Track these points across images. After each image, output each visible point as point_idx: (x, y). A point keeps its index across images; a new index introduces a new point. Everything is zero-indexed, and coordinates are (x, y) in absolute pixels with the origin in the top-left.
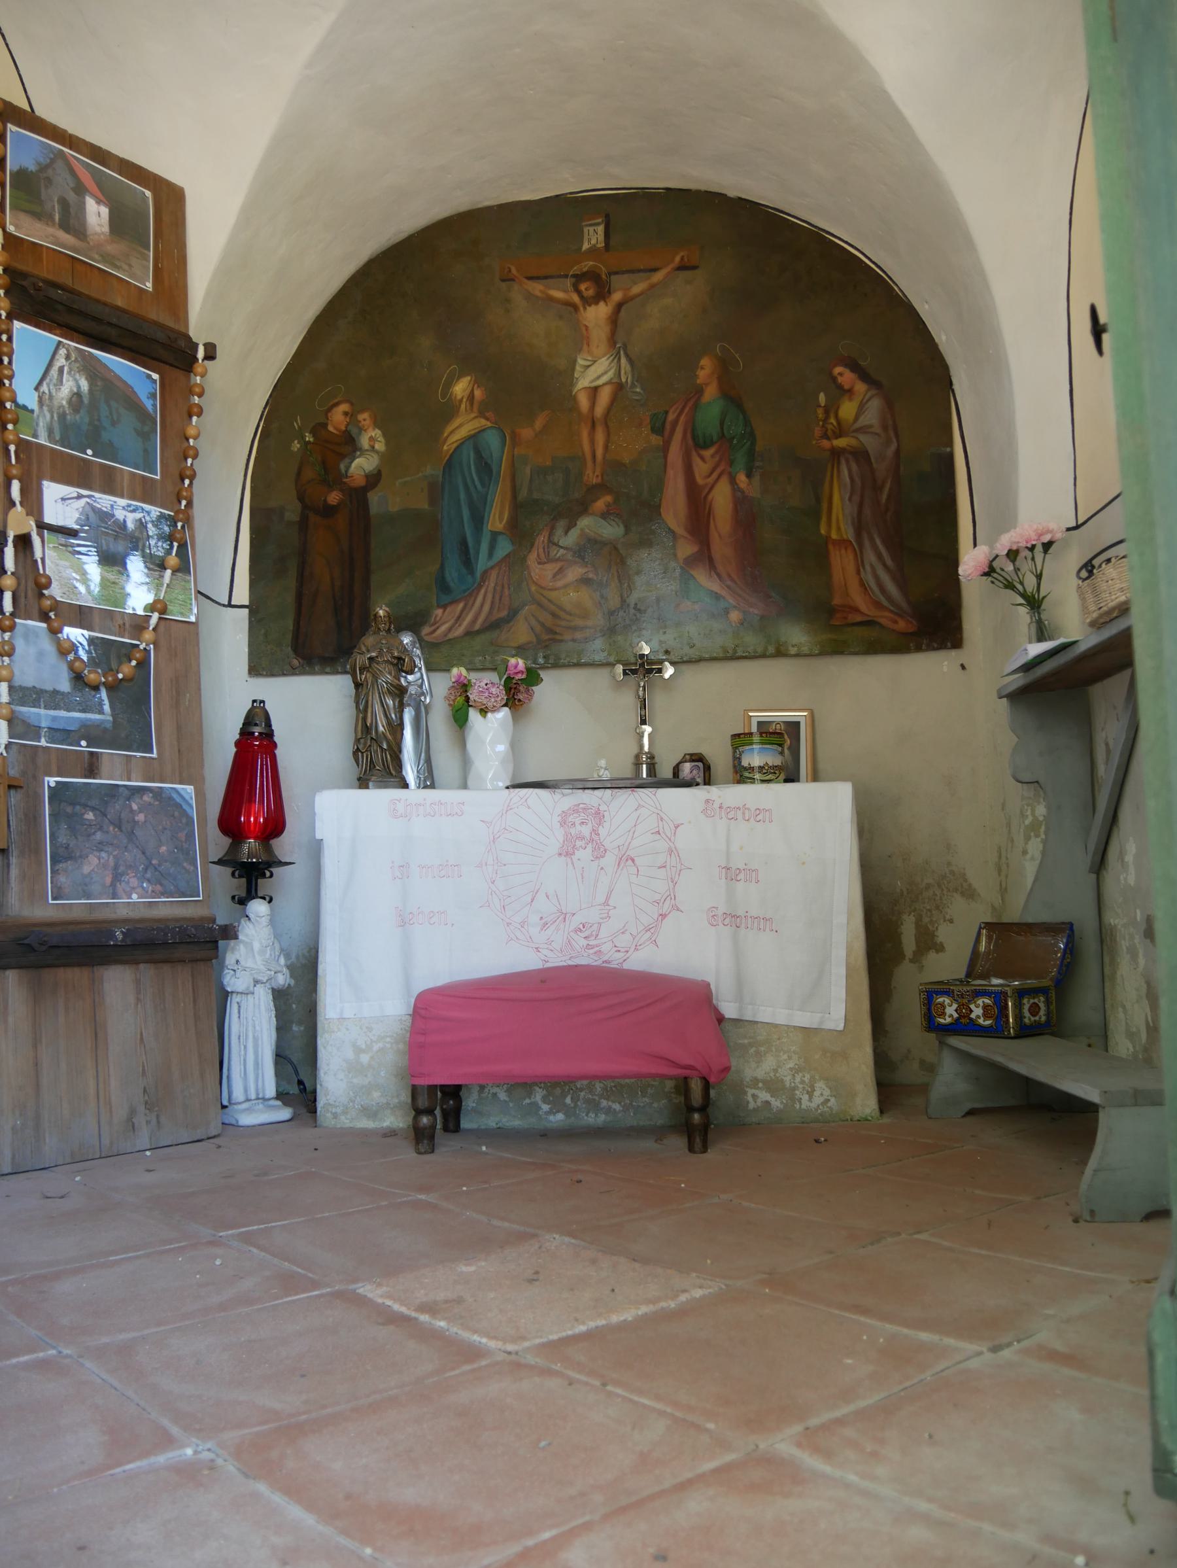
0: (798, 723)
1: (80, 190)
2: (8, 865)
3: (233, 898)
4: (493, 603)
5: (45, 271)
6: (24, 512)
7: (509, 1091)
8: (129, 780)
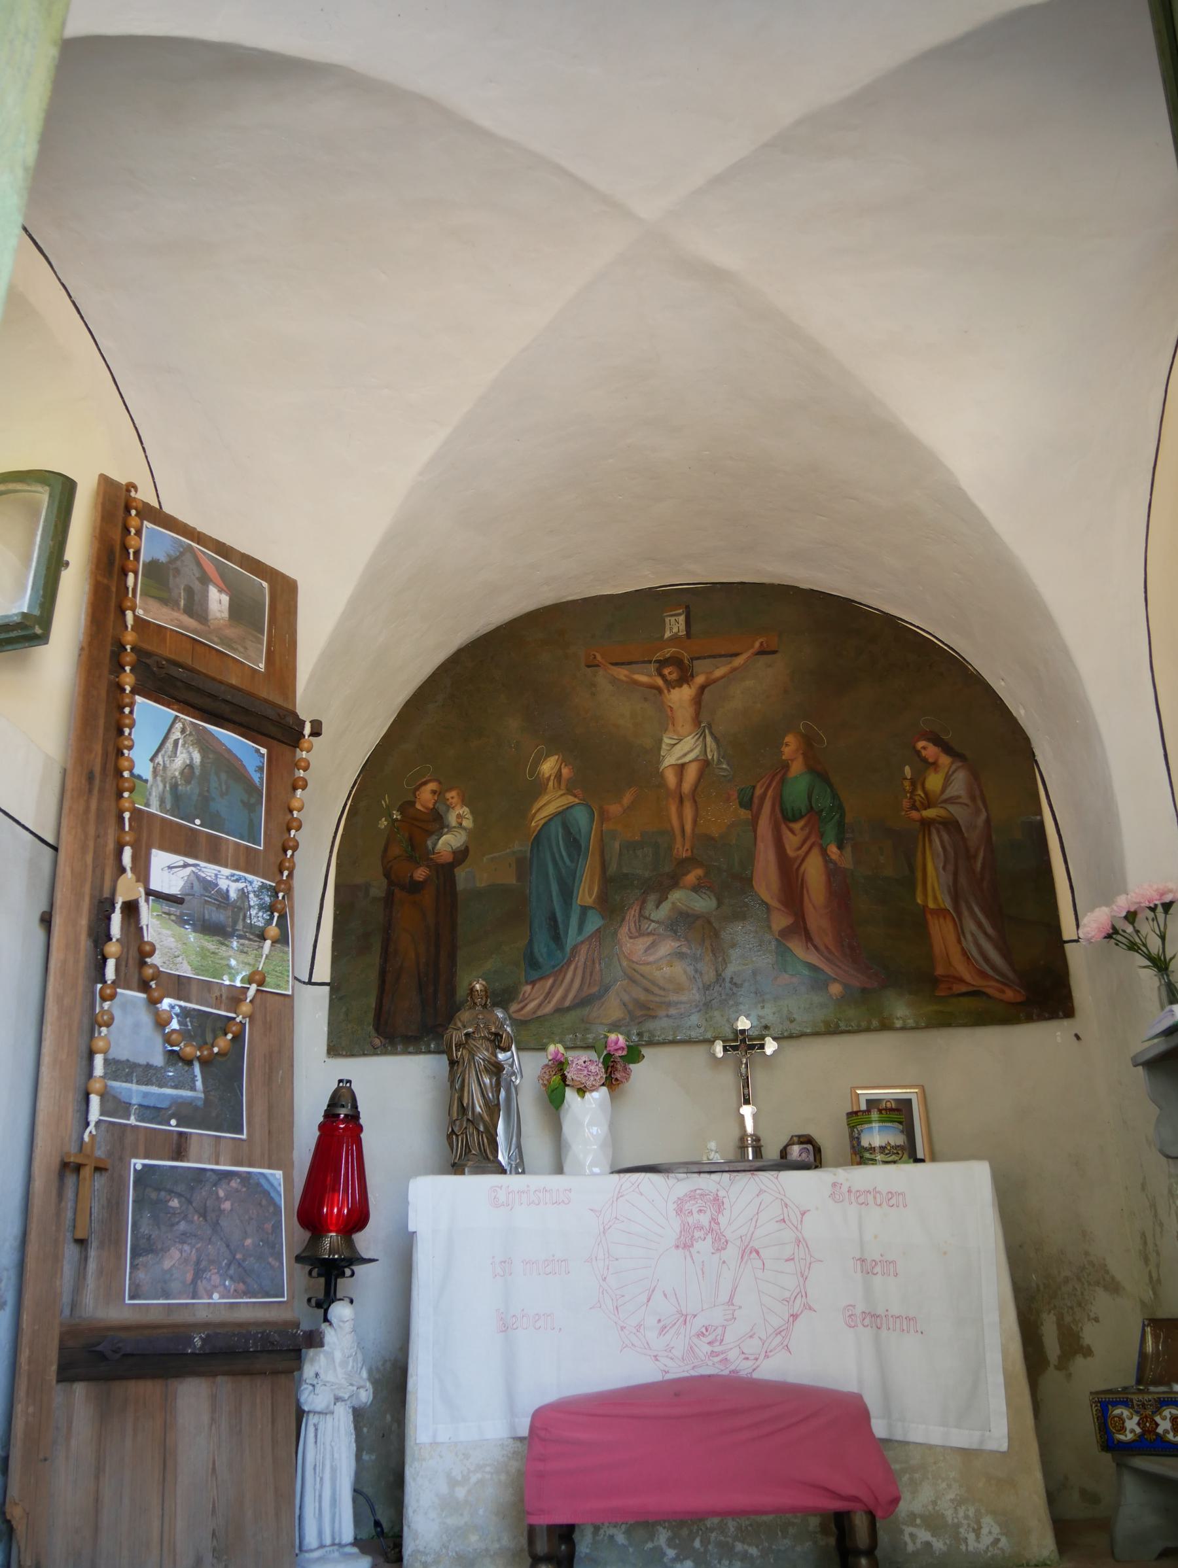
0: (910, 1101)
1: (205, 580)
2: (86, 1259)
3: (309, 1300)
4: (583, 978)
5: (167, 651)
6: (134, 878)
7: (628, 1532)
8: (217, 1163)
